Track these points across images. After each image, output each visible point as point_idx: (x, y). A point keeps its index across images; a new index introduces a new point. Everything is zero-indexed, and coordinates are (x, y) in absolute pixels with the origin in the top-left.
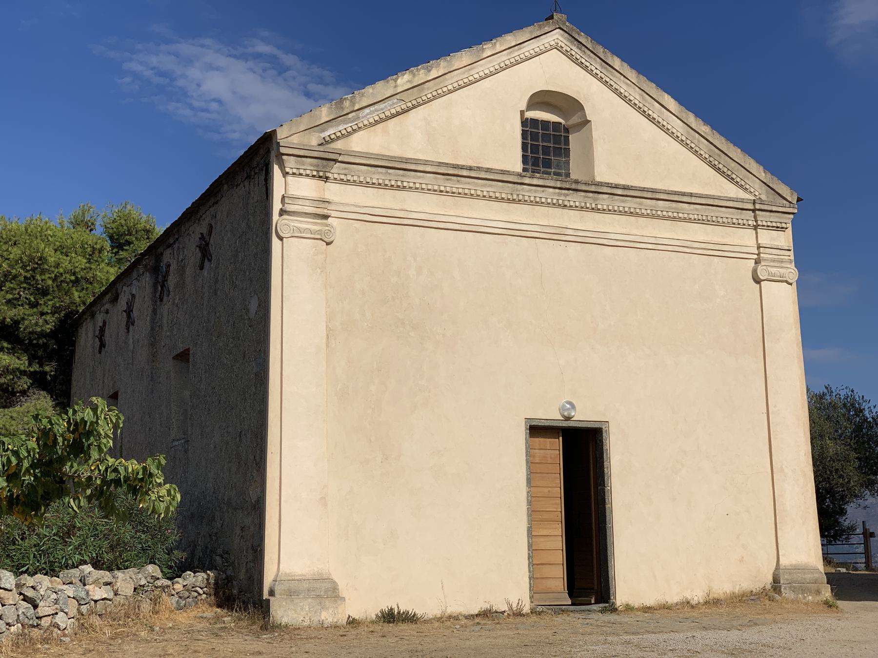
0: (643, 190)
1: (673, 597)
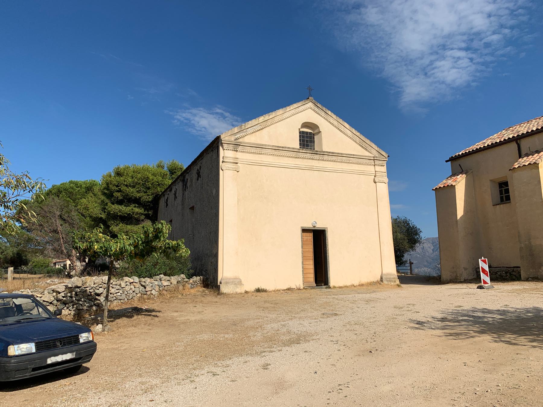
0: (338, 154)
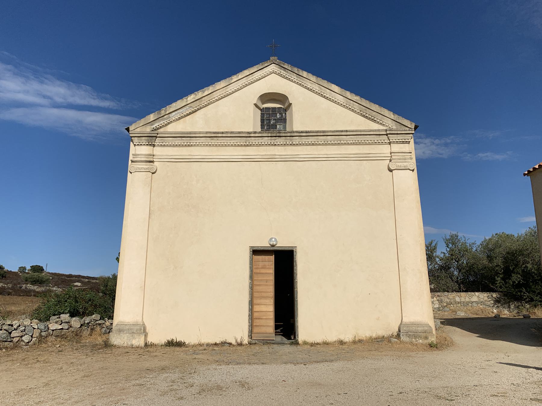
0: (317, 132)
1: (332, 338)
